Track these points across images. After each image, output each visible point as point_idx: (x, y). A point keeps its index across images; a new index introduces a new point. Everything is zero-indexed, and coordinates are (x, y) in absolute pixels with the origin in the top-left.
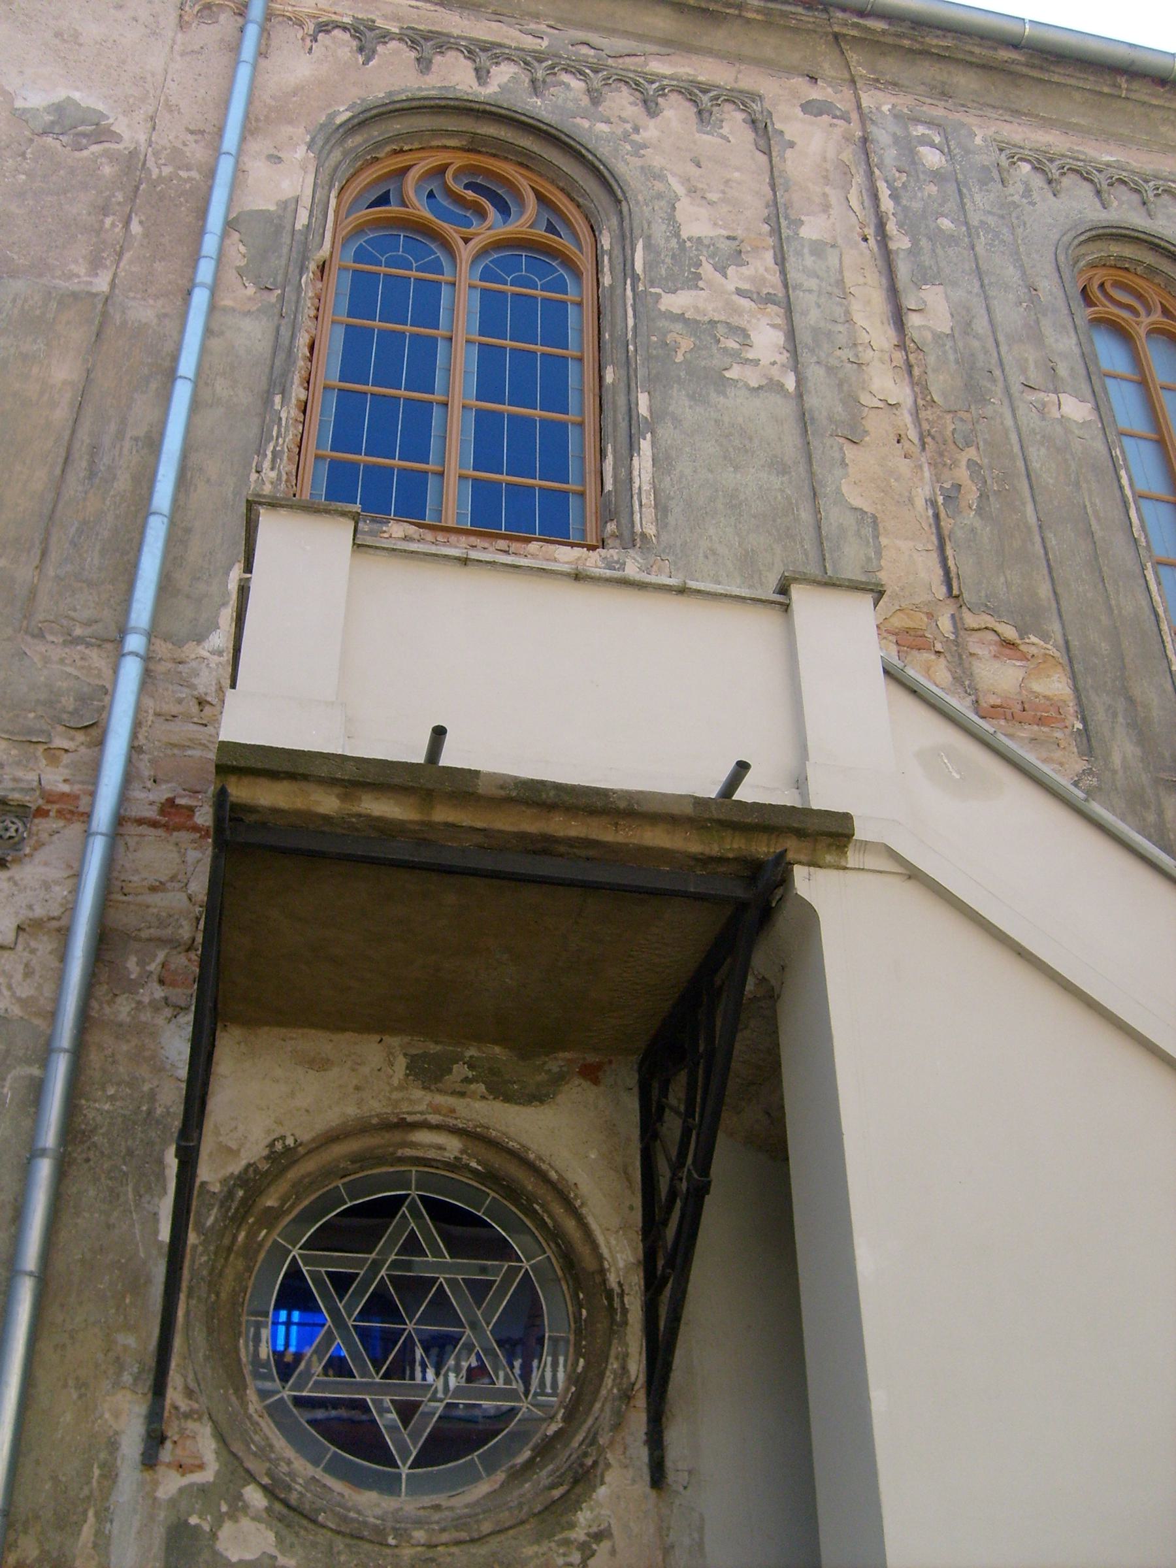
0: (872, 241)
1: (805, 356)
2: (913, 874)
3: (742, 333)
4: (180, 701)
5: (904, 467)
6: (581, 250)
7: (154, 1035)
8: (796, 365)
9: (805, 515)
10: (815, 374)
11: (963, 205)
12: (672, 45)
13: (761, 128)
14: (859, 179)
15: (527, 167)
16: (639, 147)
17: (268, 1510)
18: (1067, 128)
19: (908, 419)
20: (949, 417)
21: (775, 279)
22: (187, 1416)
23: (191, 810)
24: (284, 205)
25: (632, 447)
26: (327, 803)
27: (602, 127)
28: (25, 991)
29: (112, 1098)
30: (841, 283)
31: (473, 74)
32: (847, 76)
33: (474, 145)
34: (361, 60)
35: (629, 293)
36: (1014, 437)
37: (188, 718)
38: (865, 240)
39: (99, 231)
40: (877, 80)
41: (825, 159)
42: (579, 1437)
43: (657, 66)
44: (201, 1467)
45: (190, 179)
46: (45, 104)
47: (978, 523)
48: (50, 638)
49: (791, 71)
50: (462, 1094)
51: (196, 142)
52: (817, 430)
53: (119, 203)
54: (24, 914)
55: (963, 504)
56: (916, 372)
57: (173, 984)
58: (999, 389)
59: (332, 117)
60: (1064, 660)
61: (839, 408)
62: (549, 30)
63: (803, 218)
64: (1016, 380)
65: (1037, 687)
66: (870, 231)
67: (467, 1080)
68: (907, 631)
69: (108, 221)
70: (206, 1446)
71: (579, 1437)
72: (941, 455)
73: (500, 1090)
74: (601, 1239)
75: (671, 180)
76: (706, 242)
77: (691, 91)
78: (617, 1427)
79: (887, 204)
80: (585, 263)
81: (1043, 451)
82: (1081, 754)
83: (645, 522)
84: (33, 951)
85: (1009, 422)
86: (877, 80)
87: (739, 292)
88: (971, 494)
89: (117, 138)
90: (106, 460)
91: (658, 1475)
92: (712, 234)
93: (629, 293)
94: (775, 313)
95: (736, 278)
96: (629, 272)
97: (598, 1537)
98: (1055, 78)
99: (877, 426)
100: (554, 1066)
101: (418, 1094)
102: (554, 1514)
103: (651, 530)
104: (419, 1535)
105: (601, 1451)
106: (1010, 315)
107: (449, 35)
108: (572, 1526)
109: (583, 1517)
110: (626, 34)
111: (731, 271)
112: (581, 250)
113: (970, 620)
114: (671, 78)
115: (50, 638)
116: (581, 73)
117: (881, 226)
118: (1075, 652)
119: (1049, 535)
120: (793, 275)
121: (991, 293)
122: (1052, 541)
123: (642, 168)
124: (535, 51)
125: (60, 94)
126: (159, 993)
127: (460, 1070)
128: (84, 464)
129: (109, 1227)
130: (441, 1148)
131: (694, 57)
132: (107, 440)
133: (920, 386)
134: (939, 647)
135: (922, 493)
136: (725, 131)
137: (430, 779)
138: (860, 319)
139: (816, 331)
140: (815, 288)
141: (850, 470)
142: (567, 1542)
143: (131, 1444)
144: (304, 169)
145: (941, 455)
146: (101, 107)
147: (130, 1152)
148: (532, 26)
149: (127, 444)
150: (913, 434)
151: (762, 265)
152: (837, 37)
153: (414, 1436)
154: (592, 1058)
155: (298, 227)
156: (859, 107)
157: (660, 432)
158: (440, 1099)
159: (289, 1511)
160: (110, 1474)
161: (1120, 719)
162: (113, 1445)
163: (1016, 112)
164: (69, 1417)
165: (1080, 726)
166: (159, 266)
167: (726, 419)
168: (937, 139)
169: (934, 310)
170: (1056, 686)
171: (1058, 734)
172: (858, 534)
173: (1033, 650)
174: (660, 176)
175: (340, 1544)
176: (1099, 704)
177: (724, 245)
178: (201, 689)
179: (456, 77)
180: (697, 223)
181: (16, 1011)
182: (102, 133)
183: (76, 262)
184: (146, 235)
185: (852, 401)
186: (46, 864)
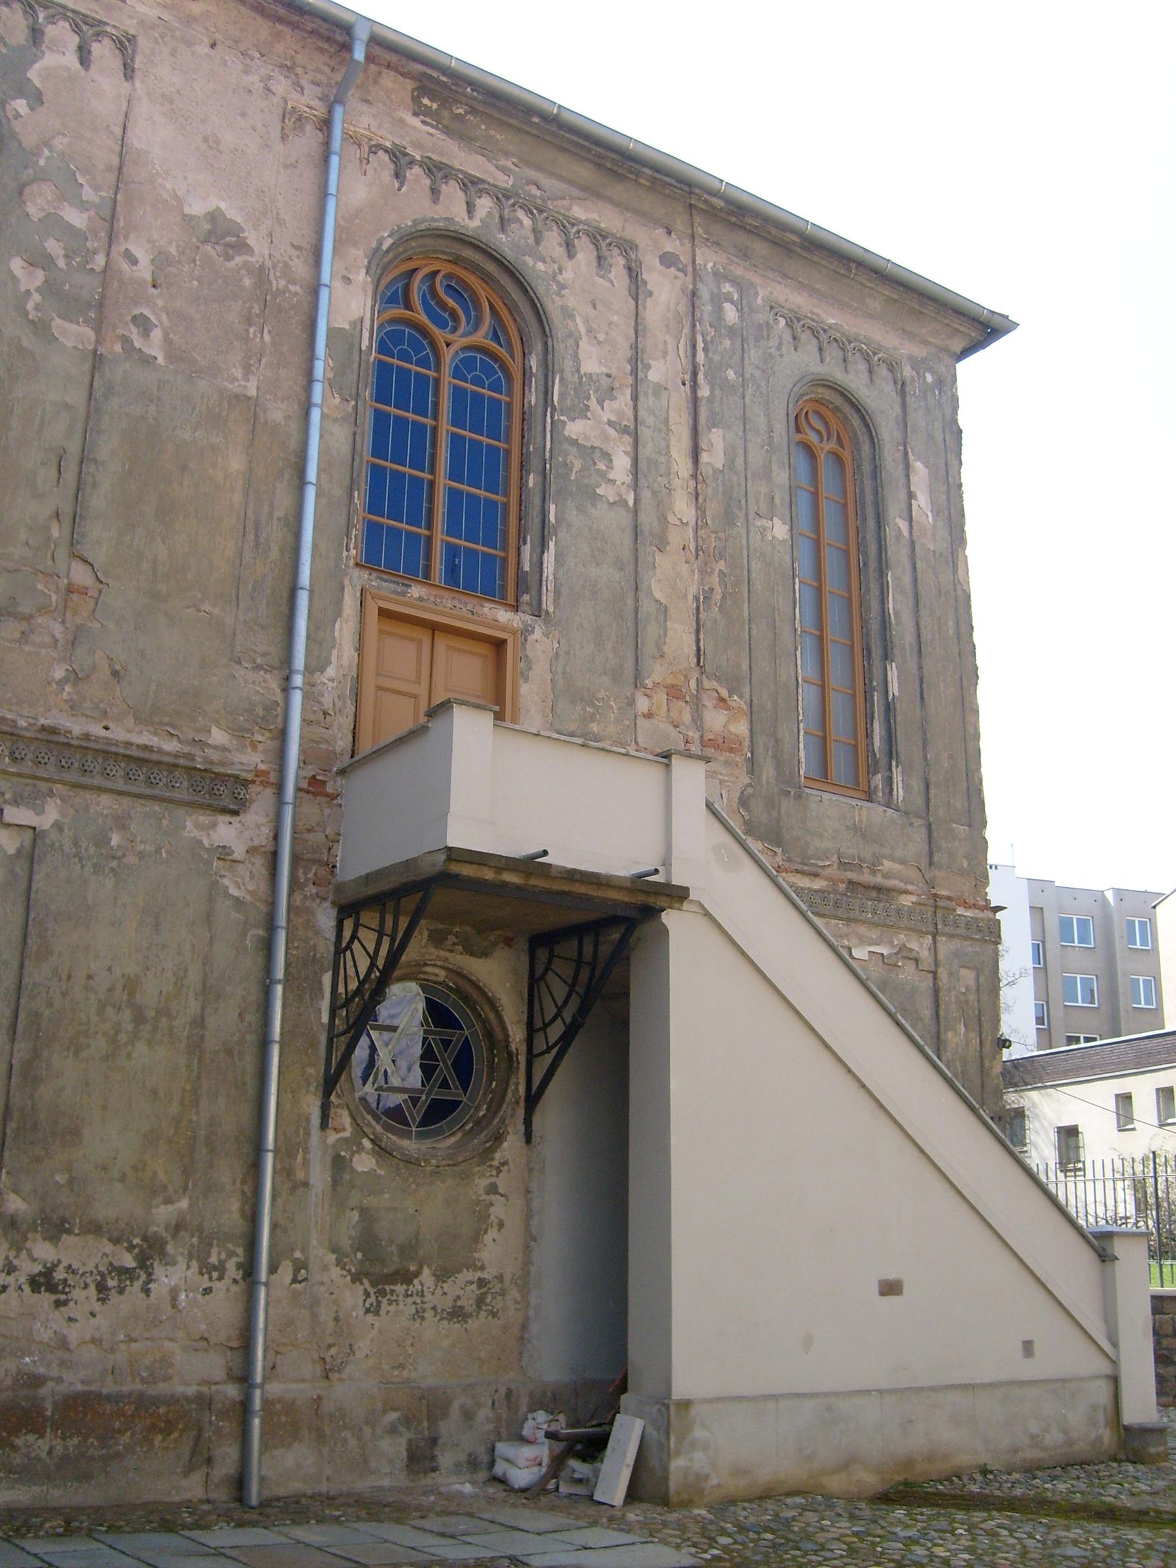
0: (688, 386)
1: (642, 482)
2: (707, 914)
3: (607, 457)
4: (315, 712)
5: (685, 568)
6: (513, 357)
7: (313, 914)
8: (635, 486)
9: (630, 602)
10: (646, 494)
11: (743, 359)
12: (591, 192)
13: (633, 273)
14: (686, 330)
15: (486, 283)
16: (562, 287)
17: (373, 1149)
18: (812, 292)
19: (691, 533)
20: (713, 536)
21: (630, 413)
22: (337, 1106)
23: (324, 782)
24: (353, 324)
25: (543, 546)
26: (489, 875)
27: (540, 266)
28: (251, 887)
29: (297, 948)
30: (667, 420)
31: (465, 207)
32: (690, 232)
33: (456, 261)
34: (397, 185)
35: (549, 420)
36: (745, 552)
37: (318, 723)
38: (684, 384)
39: (247, 339)
40: (708, 240)
41: (668, 310)
42: (497, 1120)
43: (578, 212)
44: (344, 1130)
45: (296, 294)
46: (203, 212)
47: (718, 617)
48: (245, 664)
49: (656, 222)
50: (452, 951)
51: (298, 257)
52: (643, 538)
53: (257, 315)
54: (250, 843)
55: (713, 602)
56: (700, 500)
57: (320, 885)
58: (741, 515)
59: (380, 242)
60: (748, 713)
61: (655, 524)
62: (513, 167)
63: (651, 362)
64: (752, 507)
65: (732, 728)
66: (687, 377)
67: (454, 944)
68: (673, 686)
69: (252, 330)
70: (346, 1120)
71: (497, 1120)
72: (706, 564)
73: (470, 951)
74: (509, 1028)
75: (579, 320)
76: (595, 377)
77: (597, 236)
78: (512, 1116)
79: (701, 357)
80: (516, 370)
81: (759, 565)
82: (748, 773)
83: (548, 603)
84: (253, 864)
85: (744, 542)
86: (708, 240)
87: (610, 423)
88: (717, 596)
89: (249, 250)
90: (264, 535)
91: (528, 1137)
92: (598, 371)
93: (549, 420)
94: (628, 439)
95: (607, 413)
96: (549, 402)
97: (504, 1164)
98: (815, 259)
99: (675, 538)
100: (492, 938)
101: (432, 950)
102: (486, 1155)
103: (551, 610)
104: (433, 1162)
105: (506, 1127)
106: (756, 456)
107: (452, 168)
108: (493, 1159)
109: (497, 1155)
110: (560, 178)
111: (606, 403)
112: (513, 357)
113: (707, 684)
114: (585, 223)
115: (245, 664)
116: (532, 213)
117: (695, 374)
118: (755, 708)
119: (753, 626)
120: (642, 413)
121: (749, 437)
122: (754, 632)
123: (562, 307)
124: (504, 189)
125: (213, 203)
126: (314, 890)
127: (451, 939)
128: (252, 537)
129: (300, 1015)
130: (437, 975)
131: (600, 203)
132: (263, 518)
133: (700, 510)
134: (688, 698)
135: (692, 591)
136: (612, 276)
137: (531, 865)
138: (675, 454)
139: (649, 460)
140: (652, 424)
141: (658, 571)
142: (491, 1166)
143: (316, 1120)
144: (365, 291)
145: (706, 564)
146: (239, 220)
147: (307, 977)
148: (503, 162)
149: (275, 522)
150: (692, 547)
151: (624, 399)
152: (691, 205)
153: (418, 1114)
154: (509, 934)
155: (364, 348)
156: (694, 262)
157: (560, 534)
158: (442, 953)
159: (382, 1151)
160: (308, 1133)
161: (770, 753)
162: (308, 1120)
163: (785, 276)
164: (288, 1106)
165: (749, 755)
166: (283, 372)
167: (595, 526)
168: (736, 297)
169: (716, 442)
170: (741, 728)
171: (738, 759)
172: (656, 620)
173: (734, 704)
174: (572, 317)
175: (401, 1164)
176: (761, 740)
177: (605, 381)
178: (326, 706)
179: (453, 208)
180: (590, 366)
181: (248, 898)
182: (241, 246)
183: (235, 367)
184: (273, 344)
185: (663, 519)
186: (256, 813)
